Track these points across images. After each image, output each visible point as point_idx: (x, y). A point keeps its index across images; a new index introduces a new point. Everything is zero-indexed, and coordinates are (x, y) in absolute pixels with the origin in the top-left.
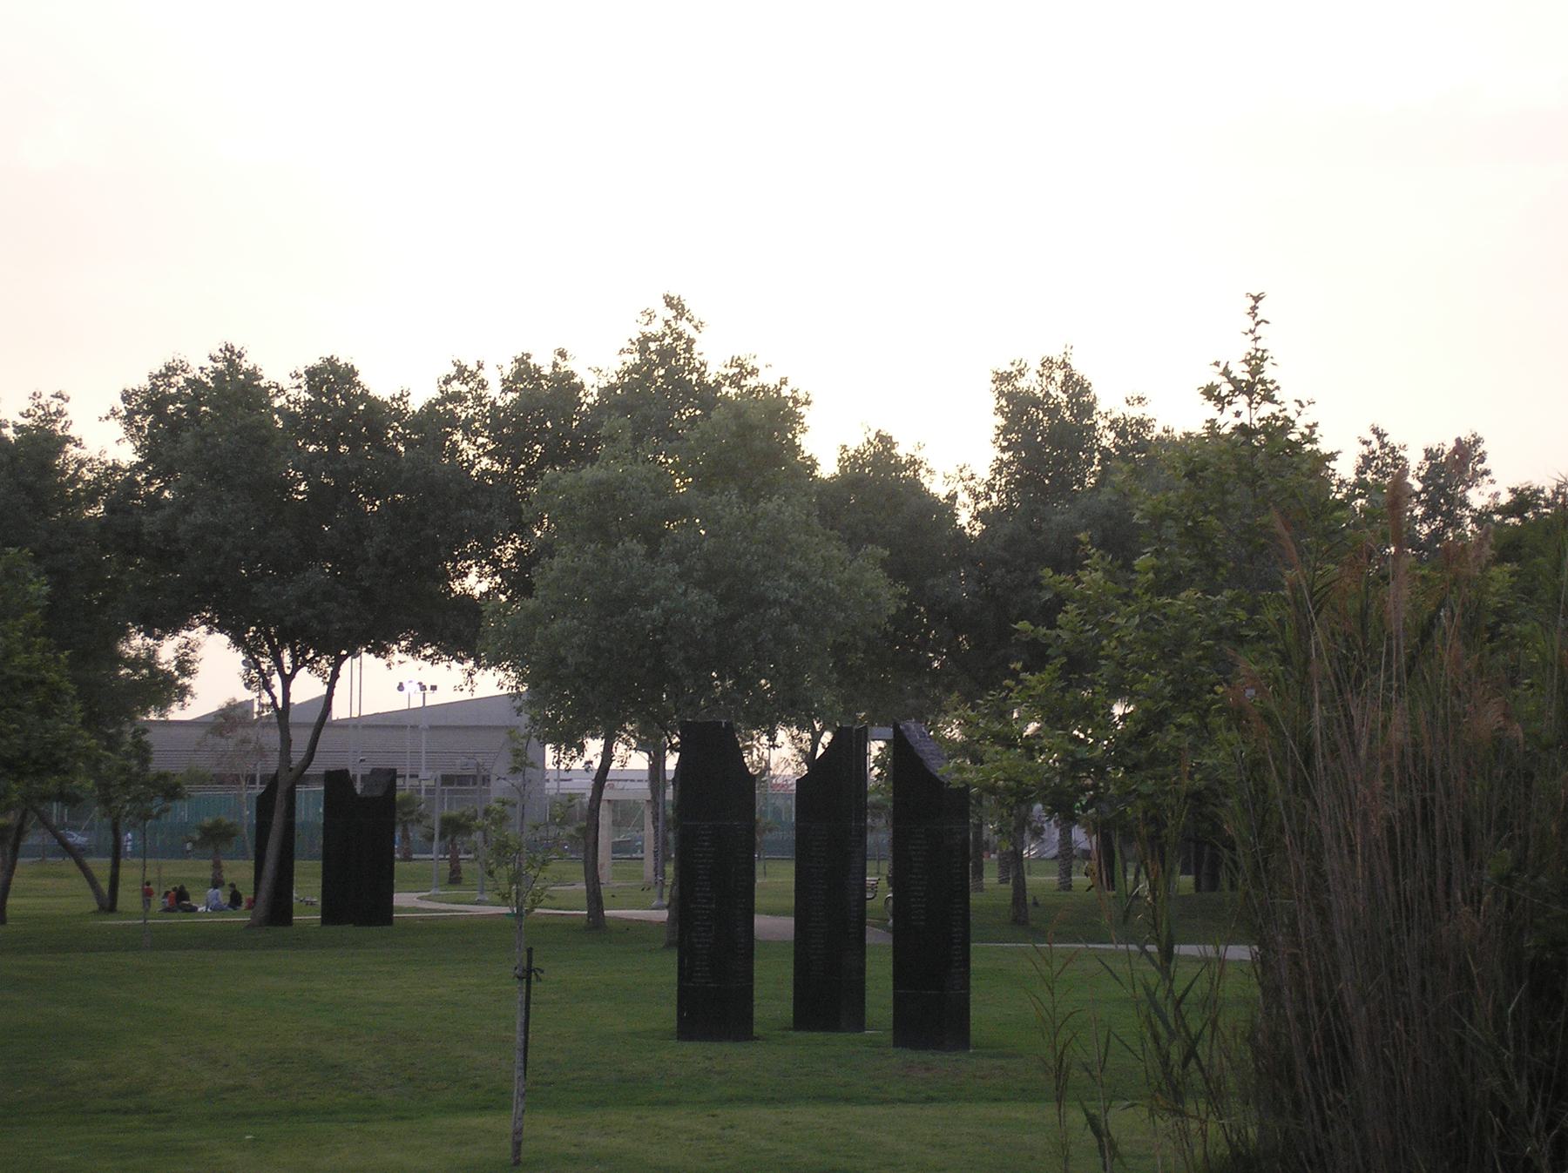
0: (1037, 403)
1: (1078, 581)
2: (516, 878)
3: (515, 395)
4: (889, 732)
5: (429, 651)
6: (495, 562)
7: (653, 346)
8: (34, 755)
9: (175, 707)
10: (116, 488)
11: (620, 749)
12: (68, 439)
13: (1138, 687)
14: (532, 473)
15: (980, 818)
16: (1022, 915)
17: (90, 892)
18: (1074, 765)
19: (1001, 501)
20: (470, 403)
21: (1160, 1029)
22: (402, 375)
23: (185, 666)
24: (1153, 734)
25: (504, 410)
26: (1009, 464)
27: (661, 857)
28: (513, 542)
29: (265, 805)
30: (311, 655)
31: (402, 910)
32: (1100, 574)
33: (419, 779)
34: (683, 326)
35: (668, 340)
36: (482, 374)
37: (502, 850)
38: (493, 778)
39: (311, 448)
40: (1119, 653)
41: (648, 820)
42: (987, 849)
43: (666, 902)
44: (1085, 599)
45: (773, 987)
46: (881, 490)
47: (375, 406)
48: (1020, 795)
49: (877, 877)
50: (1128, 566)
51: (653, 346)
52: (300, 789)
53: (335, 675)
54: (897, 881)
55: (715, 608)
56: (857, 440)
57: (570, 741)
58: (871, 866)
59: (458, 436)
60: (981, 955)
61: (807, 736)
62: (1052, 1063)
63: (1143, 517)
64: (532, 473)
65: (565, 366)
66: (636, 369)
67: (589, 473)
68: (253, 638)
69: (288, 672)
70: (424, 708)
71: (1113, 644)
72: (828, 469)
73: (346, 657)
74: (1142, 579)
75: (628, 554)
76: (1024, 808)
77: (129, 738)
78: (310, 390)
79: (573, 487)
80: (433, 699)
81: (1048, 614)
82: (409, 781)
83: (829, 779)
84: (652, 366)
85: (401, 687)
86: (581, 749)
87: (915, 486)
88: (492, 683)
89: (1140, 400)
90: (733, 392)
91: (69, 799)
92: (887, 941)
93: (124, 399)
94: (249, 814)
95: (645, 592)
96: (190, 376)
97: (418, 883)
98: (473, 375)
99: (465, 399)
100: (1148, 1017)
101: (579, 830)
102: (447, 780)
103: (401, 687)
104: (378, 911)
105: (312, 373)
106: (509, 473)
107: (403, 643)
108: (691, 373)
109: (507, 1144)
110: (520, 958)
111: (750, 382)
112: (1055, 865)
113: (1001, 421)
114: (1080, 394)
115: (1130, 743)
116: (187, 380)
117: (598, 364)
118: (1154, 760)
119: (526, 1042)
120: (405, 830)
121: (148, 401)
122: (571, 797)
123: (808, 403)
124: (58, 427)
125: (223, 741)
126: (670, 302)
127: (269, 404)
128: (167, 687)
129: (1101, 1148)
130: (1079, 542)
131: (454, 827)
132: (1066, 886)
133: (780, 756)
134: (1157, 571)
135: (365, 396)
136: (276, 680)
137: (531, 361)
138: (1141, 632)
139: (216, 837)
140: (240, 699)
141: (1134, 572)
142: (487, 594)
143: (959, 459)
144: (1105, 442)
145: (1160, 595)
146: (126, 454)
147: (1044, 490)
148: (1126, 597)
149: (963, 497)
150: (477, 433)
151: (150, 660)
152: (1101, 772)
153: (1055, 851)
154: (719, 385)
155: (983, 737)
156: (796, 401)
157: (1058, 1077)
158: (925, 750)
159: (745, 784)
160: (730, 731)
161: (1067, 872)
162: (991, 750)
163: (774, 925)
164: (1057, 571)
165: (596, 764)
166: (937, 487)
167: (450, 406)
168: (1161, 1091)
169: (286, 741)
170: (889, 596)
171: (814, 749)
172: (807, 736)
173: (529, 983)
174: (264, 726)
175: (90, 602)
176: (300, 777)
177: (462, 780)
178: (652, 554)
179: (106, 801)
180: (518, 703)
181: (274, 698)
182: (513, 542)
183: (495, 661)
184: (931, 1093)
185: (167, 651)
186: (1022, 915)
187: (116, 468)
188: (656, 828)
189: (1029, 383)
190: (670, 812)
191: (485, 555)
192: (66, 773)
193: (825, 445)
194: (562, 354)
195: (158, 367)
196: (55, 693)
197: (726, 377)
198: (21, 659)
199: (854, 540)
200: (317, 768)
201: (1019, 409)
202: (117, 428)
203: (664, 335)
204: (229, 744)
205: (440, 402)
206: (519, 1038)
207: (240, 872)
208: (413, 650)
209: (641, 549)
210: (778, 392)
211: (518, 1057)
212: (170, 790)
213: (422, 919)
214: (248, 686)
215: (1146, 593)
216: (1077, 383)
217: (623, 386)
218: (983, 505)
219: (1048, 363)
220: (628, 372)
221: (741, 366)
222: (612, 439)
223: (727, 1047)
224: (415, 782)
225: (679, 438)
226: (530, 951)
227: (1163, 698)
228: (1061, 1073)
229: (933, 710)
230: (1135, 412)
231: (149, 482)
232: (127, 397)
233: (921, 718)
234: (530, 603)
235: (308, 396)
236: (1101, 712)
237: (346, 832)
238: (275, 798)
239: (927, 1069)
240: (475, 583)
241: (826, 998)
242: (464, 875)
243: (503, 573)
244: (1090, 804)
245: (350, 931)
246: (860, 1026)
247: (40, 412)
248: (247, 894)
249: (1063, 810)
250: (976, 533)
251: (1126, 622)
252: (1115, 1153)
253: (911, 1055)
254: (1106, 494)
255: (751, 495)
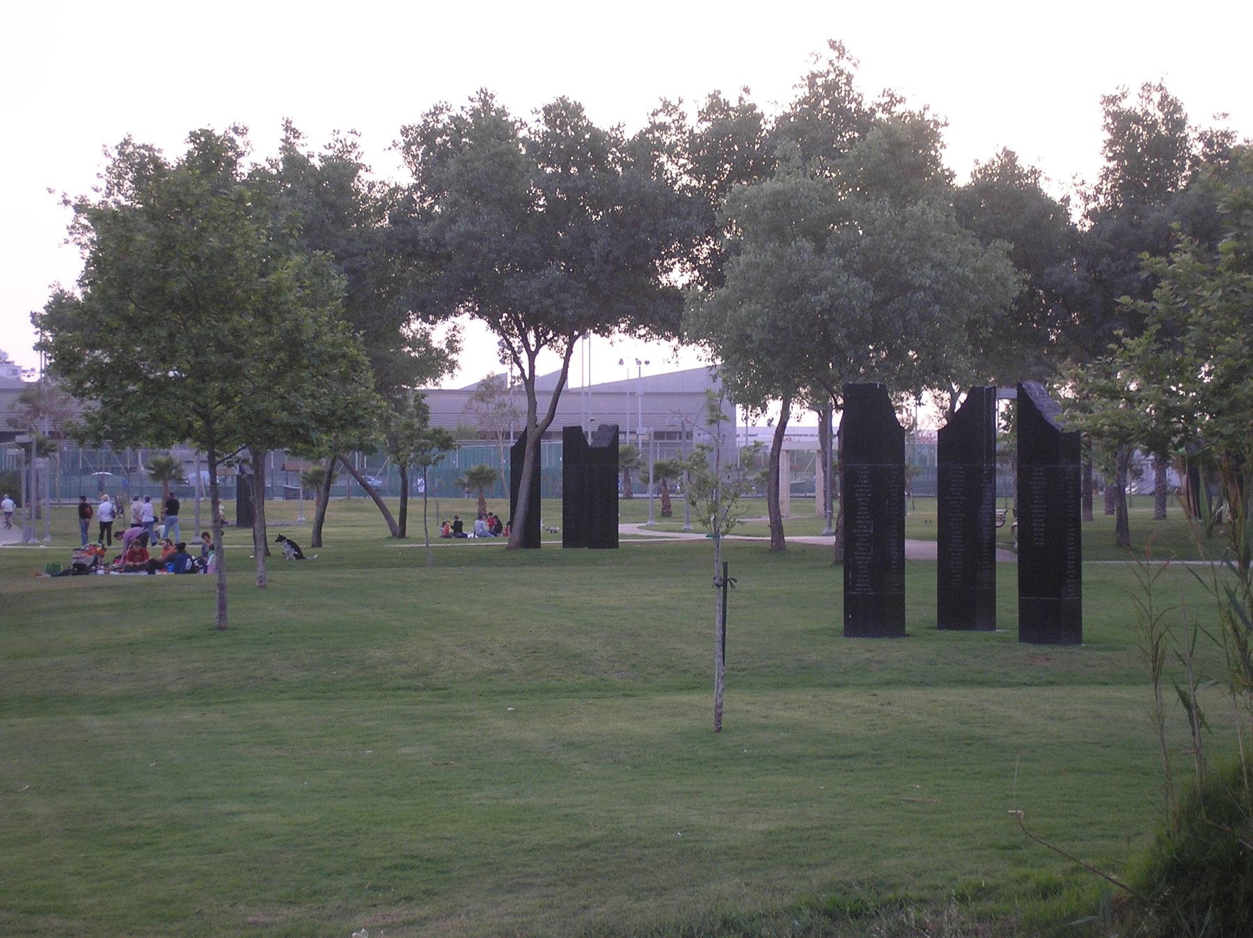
0: (1137, 120)
1: (1171, 262)
2: (714, 508)
3: (709, 124)
4: (1014, 392)
5: (643, 332)
6: (694, 260)
7: (820, 81)
8: (339, 412)
9: (446, 376)
10: (399, 206)
11: (795, 409)
12: (360, 166)
13: (1219, 348)
14: (723, 188)
15: (1090, 462)
16: (1123, 539)
17: (386, 523)
18: (1167, 412)
19: (1107, 202)
20: (673, 131)
21: (1239, 621)
22: (618, 112)
23: (452, 344)
24: (1233, 386)
25: (700, 137)
26: (1113, 172)
27: (829, 497)
28: (708, 243)
29: (517, 454)
30: (550, 335)
31: (626, 536)
32: (1188, 257)
33: (636, 435)
34: (844, 64)
35: (832, 76)
36: (682, 108)
37: (703, 486)
38: (695, 434)
39: (549, 170)
40: (1204, 320)
41: (819, 465)
42: (1096, 487)
43: (833, 530)
44: (1175, 276)
45: (921, 595)
46: (1007, 199)
47: (597, 135)
48: (1122, 438)
49: (1005, 510)
50: (1212, 249)
51: (820, 81)
52: (544, 443)
53: (569, 351)
54: (1021, 513)
55: (871, 293)
56: (988, 155)
57: (755, 401)
58: (999, 502)
59: (664, 158)
60: (1090, 571)
61: (947, 395)
62: (1149, 651)
63: (1226, 207)
64: (723, 188)
65: (749, 100)
66: (805, 100)
67: (769, 185)
68: (506, 323)
69: (533, 349)
70: (641, 380)
71: (1200, 313)
72: (962, 180)
73: (577, 337)
74: (1224, 258)
75: (799, 251)
76: (1125, 447)
77: (411, 402)
78: (547, 122)
79: (756, 197)
80: (647, 372)
81: (1145, 292)
82: (629, 437)
83: (965, 431)
84: (819, 98)
85: (621, 362)
86: (764, 409)
87: (1035, 192)
88: (694, 358)
89: (1225, 115)
90: (885, 116)
91: (368, 450)
92: (1014, 559)
93: (402, 133)
94: (505, 463)
95: (813, 281)
96: (454, 114)
97: (638, 516)
98: (675, 108)
99: (670, 128)
100: (1229, 612)
101: (763, 474)
102: (659, 435)
103: (621, 362)
104: (606, 537)
105: (548, 110)
106: (704, 187)
107: (623, 326)
108: (850, 102)
109: (711, 715)
110: (717, 571)
111: (898, 109)
112: (1153, 500)
113: (1108, 136)
114: (1175, 112)
115: (1214, 393)
116: (451, 117)
117: (775, 99)
118: (1234, 407)
119: (724, 635)
120: (627, 475)
121: (421, 134)
122: (757, 444)
123: (946, 125)
124: (353, 156)
125: (484, 405)
126: (833, 45)
127: (515, 135)
128: (437, 362)
129: (1191, 717)
130: (1171, 229)
131: (664, 472)
132: (1161, 515)
133: (925, 414)
134: (1237, 252)
135: (589, 128)
136: (524, 357)
137: (721, 97)
138: (1224, 303)
139: (481, 480)
140: (497, 373)
141: (1217, 253)
142: (688, 285)
143: (1074, 172)
144: (1194, 151)
145: (1240, 271)
146: (406, 178)
147: (1144, 192)
148: (1213, 275)
149: (1076, 200)
150: (679, 155)
151: (425, 339)
152: (1190, 418)
153: (1152, 488)
154: (873, 111)
155: (1091, 391)
156: (937, 124)
157: (1154, 662)
158: (1043, 404)
159: (897, 435)
160: (883, 393)
161: (1162, 505)
162: (1098, 402)
163: (921, 547)
164: (1153, 255)
165: (776, 423)
166: (1053, 190)
167: (657, 134)
168: (1239, 671)
169: (533, 405)
170: (1015, 283)
171: (953, 406)
172: (947, 395)
173: (725, 587)
174: (516, 393)
175: (380, 295)
176: (543, 434)
177: (671, 435)
178: (820, 250)
179: (395, 451)
180: (713, 372)
181: (522, 370)
182: (708, 243)
183: (694, 339)
184: (1051, 678)
185: (439, 334)
186: (1123, 539)
187: (397, 189)
188: (825, 472)
189: (1132, 104)
190: (836, 459)
191: (686, 254)
192: (364, 427)
193: (961, 160)
194: (746, 90)
195: (428, 108)
196: (354, 365)
197: (879, 105)
198: (328, 338)
199: (985, 237)
200: (557, 426)
201: (1123, 125)
202: (398, 156)
203: (828, 72)
204: (488, 407)
205: (649, 131)
206: (718, 633)
207: (500, 507)
208: (630, 330)
209: (809, 246)
210: (922, 115)
211: (718, 647)
212: (446, 442)
213: (641, 543)
214: (503, 362)
215: (1228, 269)
216: (1171, 103)
217: (795, 116)
218: (1092, 205)
219: (1147, 87)
220: (800, 103)
221: (892, 96)
222: (786, 159)
223: (884, 642)
224: (634, 437)
225: (841, 155)
226: (725, 565)
227: (1242, 357)
228: (1157, 659)
229: (1050, 373)
230: (1220, 126)
231: (422, 199)
232: (405, 131)
233: (1040, 379)
234: (723, 292)
235: (545, 128)
236: (1190, 369)
237: (581, 479)
238: (524, 449)
239: (1047, 660)
240: (678, 276)
241: (964, 603)
242: (673, 509)
243: (699, 268)
244: (1181, 444)
245: (585, 552)
246: (990, 624)
247: (339, 145)
248: (505, 521)
249: (1158, 445)
250: (1086, 229)
251: (1211, 294)
252: (1202, 722)
253: (1032, 648)
254: (1196, 189)
255: (900, 200)
